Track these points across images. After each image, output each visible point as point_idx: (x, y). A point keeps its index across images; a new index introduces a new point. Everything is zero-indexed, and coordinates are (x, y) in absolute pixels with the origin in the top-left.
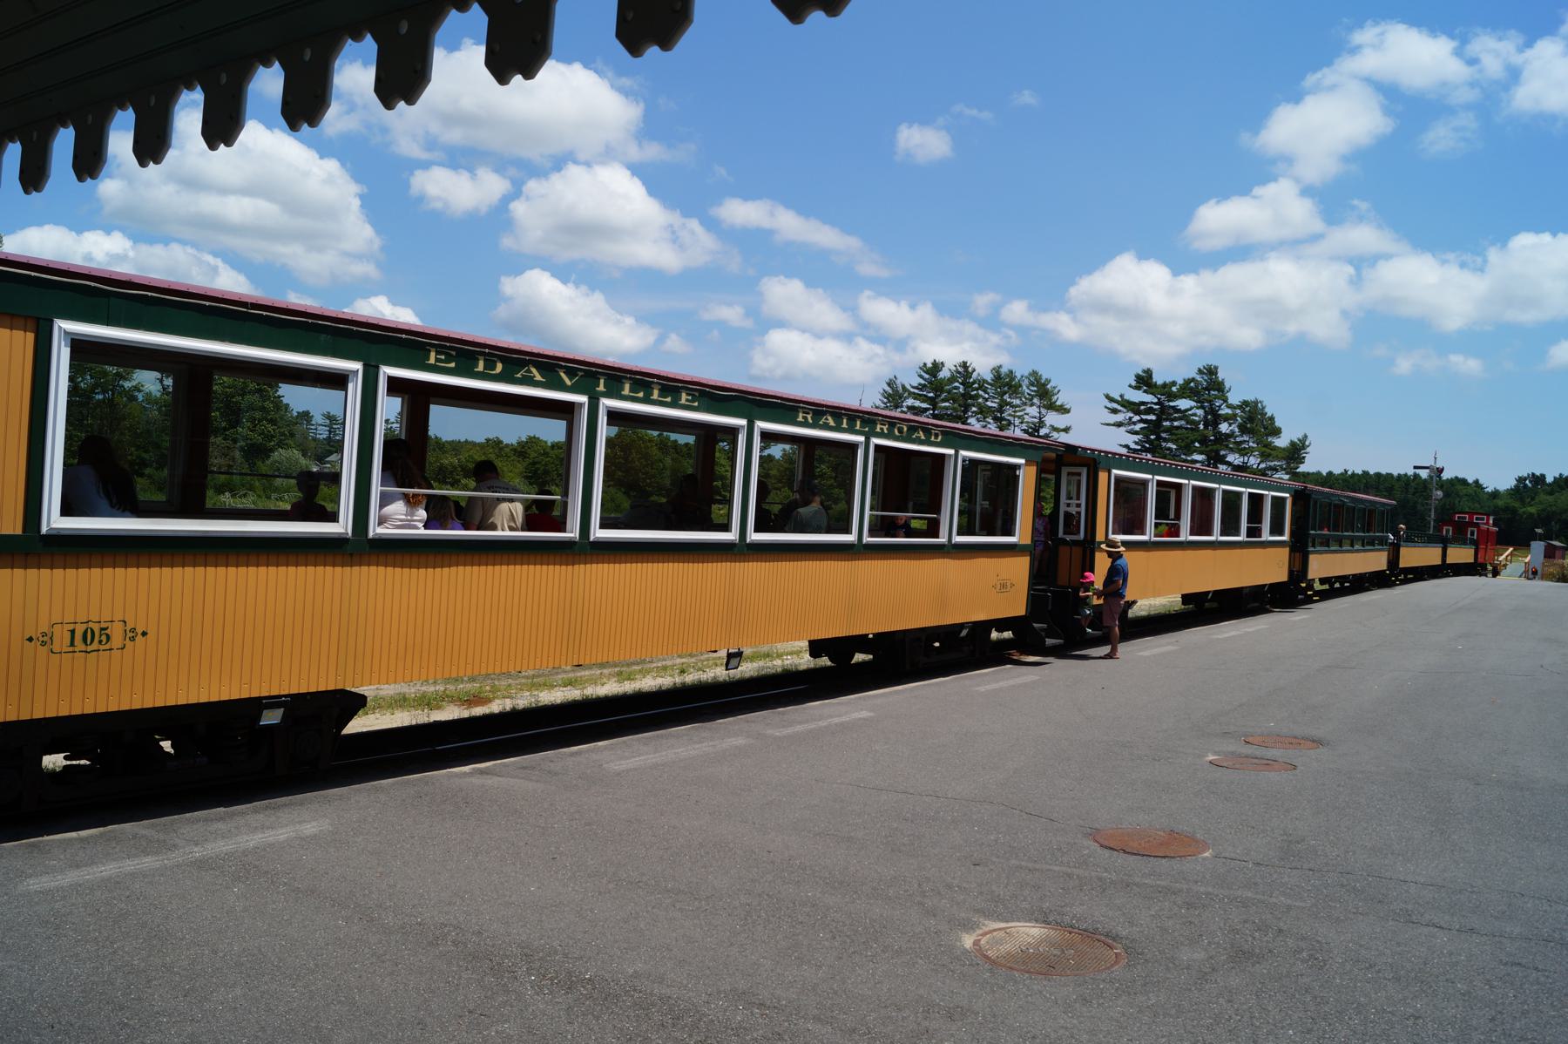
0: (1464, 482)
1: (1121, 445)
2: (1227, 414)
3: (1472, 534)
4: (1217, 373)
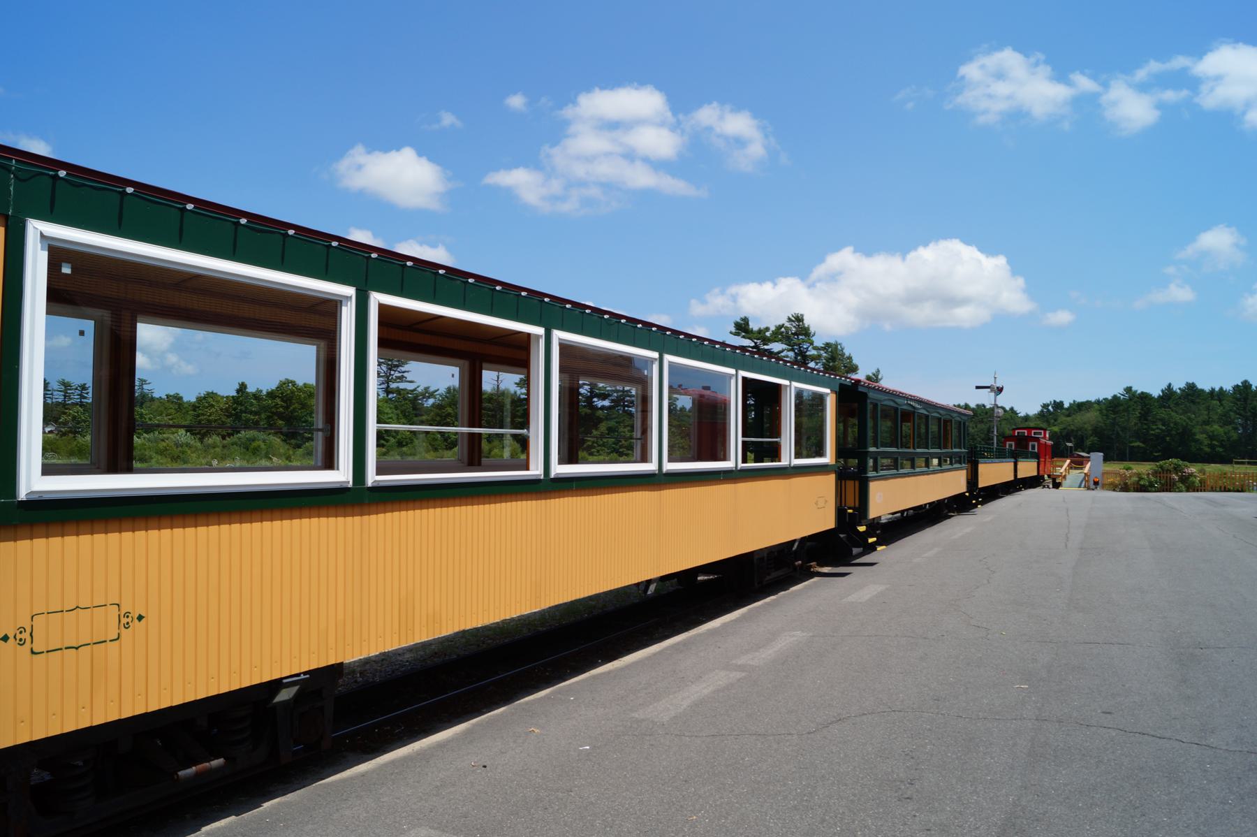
2: (813, 354)
3: (1033, 447)
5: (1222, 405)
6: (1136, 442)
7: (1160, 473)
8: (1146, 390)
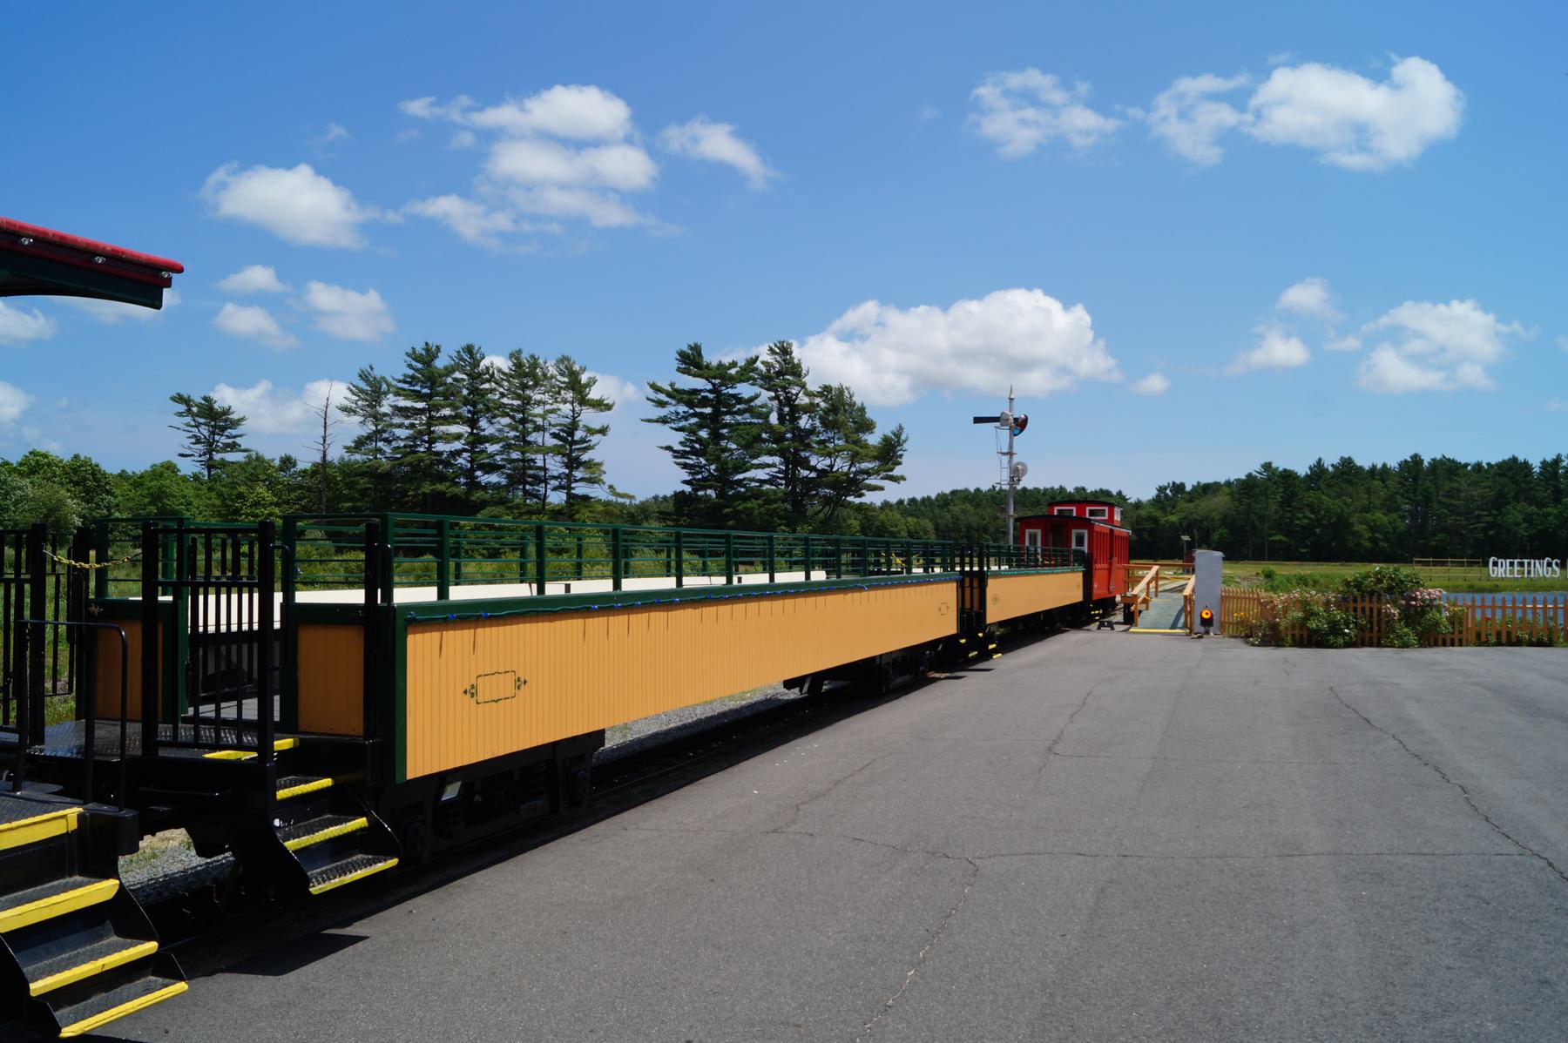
1: (661, 448)
3: (1080, 541)
4: (791, 353)
5: (1386, 486)
6: (1277, 534)
7: (1355, 601)
8: (1289, 467)
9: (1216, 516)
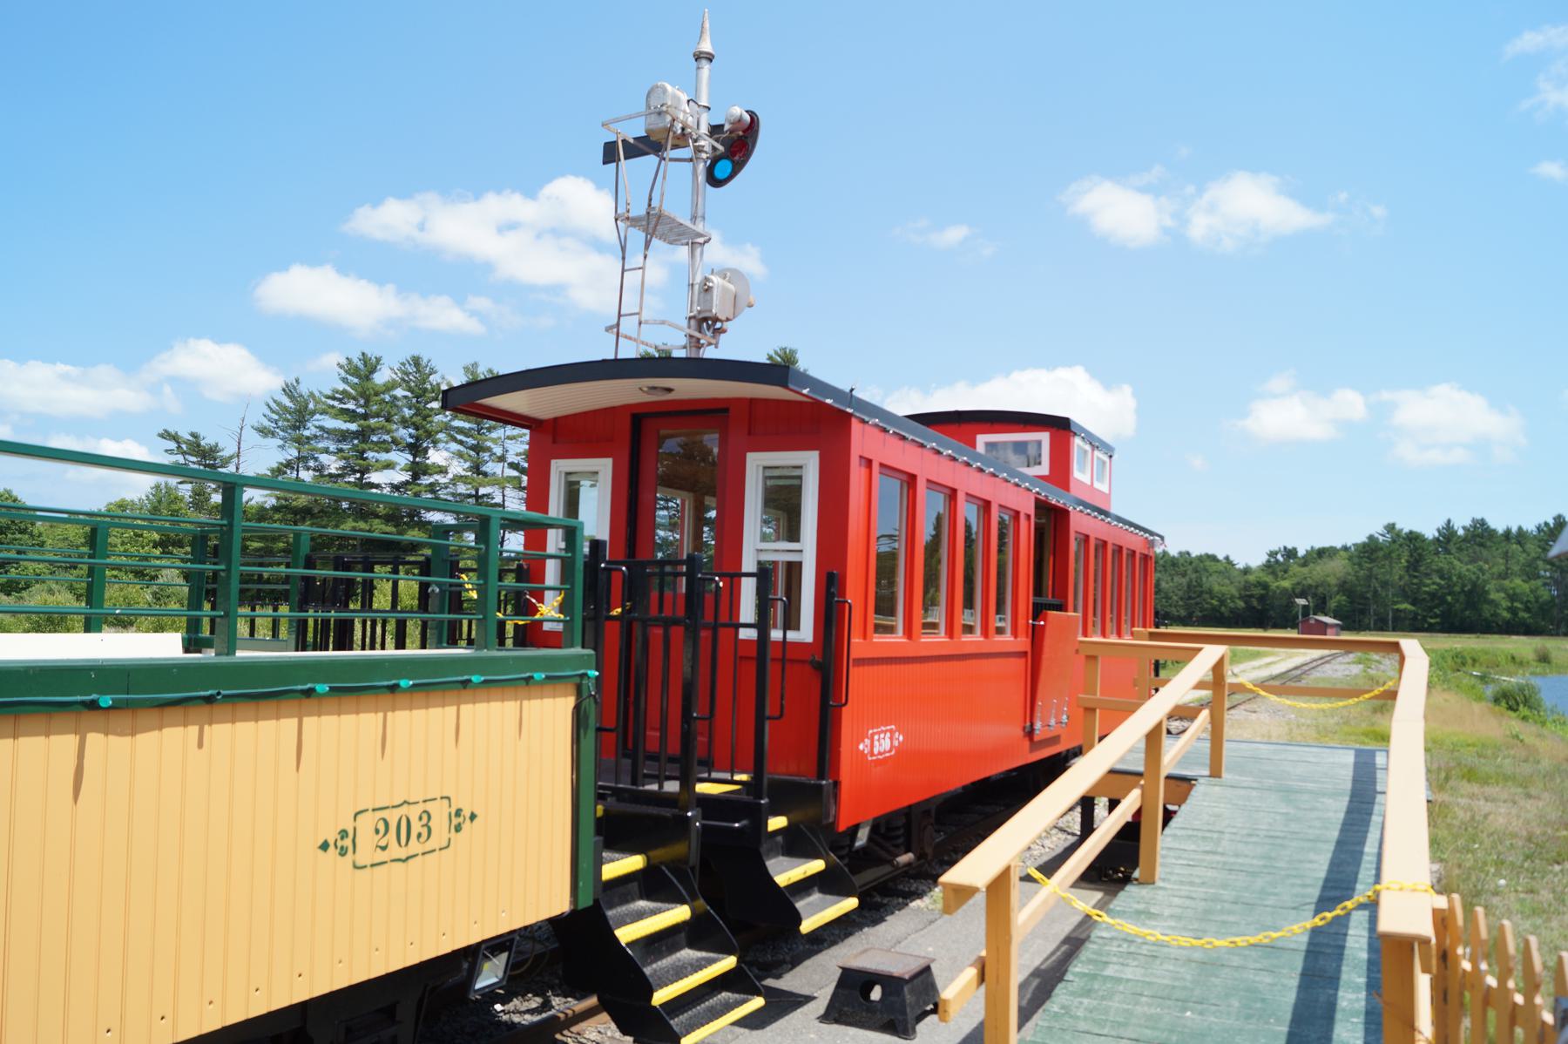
0: (1213, 558)
3: (783, 502)
9: (1333, 581)
